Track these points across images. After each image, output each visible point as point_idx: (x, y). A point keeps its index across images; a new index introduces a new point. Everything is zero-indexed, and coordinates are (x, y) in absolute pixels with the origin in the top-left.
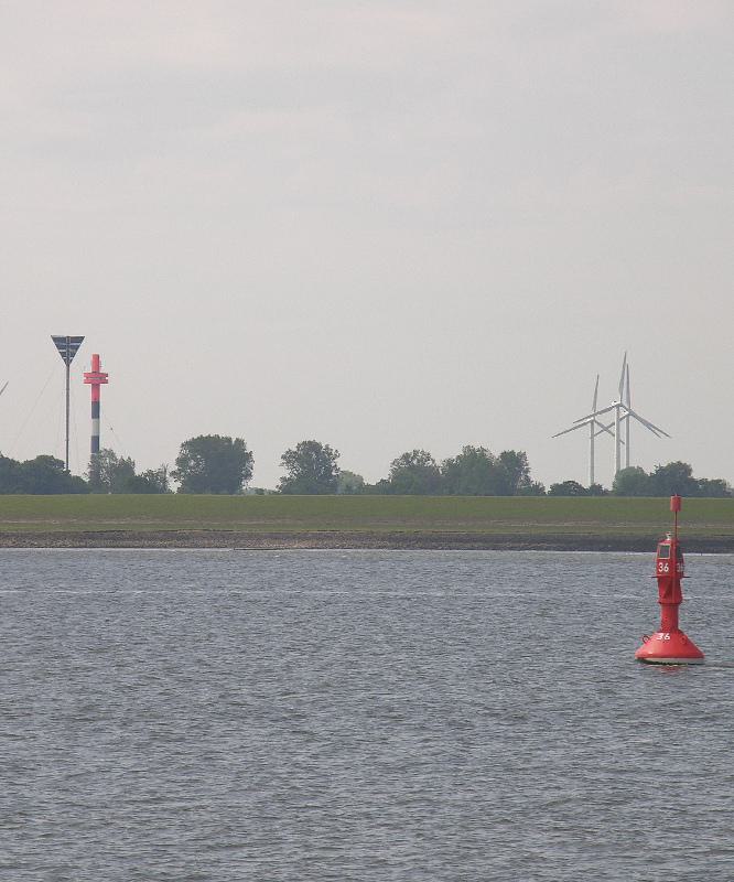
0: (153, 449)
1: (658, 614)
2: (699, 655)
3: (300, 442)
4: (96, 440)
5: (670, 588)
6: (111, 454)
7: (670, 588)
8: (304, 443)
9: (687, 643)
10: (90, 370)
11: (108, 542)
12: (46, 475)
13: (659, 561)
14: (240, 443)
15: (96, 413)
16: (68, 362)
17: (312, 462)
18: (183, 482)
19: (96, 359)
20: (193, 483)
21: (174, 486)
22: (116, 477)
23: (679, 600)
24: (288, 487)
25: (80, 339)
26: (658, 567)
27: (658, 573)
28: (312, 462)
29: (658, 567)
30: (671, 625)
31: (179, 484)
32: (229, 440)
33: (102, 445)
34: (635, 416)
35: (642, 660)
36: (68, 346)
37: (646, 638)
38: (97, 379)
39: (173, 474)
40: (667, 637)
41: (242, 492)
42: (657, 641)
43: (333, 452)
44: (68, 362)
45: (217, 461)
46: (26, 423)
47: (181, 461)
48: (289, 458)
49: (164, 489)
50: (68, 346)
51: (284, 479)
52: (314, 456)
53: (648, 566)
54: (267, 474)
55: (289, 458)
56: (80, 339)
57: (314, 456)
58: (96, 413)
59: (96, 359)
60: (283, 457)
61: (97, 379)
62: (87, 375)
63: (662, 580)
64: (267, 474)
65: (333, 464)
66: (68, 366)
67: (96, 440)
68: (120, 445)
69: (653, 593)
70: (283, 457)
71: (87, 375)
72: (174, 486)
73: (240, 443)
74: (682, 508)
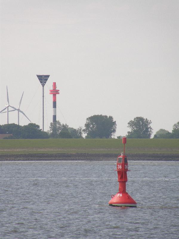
0: (76, 119)
1: (118, 186)
2: (135, 203)
3: (88, 117)
4: (55, 117)
5: (123, 175)
6: (59, 123)
7: (123, 175)
8: (137, 118)
9: (129, 197)
10: (52, 89)
11: (54, 158)
12: (32, 131)
13: (118, 164)
14: (111, 118)
15: (55, 106)
16: (43, 86)
17: (140, 126)
18: (88, 134)
19: (55, 84)
20: (92, 134)
21: (84, 135)
22: (64, 133)
23: (126, 180)
24: (130, 135)
25: (48, 76)
26: (118, 167)
27: (118, 169)
28: (140, 126)
29: (118, 167)
30: (123, 190)
31: (86, 135)
32: (106, 117)
33: (57, 120)
34: (10, 106)
35: (111, 205)
36: (43, 79)
37: (112, 196)
38: (55, 92)
39: (84, 130)
40: (121, 195)
41: (111, 138)
42: (118, 197)
43: (149, 121)
44: (43, 86)
45: (102, 125)
46: (35, 113)
47: (87, 125)
48: (131, 124)
49: (81, 137)
50: (43, 79)
51: (129, 132)
52: (141, 123)
53: (112, 167)
54: (122, 130)
55: (131, 124)
56: (48, 76)
57: (141, 123)
58: (55, 106)
59: (55, 84)
60: (129, 123)
61: (55, 92)
62: (51, 91)
63: (119, 172)
64: (122, 130)
65: (149, 126)
66: (43, 87)
67: (55, 117)
68: (62, 120)
69: (116, 178)
70: (129, 123)
71: (51, 91)
72: (84, 135)
73: (111, 118)
74: (127, 142)
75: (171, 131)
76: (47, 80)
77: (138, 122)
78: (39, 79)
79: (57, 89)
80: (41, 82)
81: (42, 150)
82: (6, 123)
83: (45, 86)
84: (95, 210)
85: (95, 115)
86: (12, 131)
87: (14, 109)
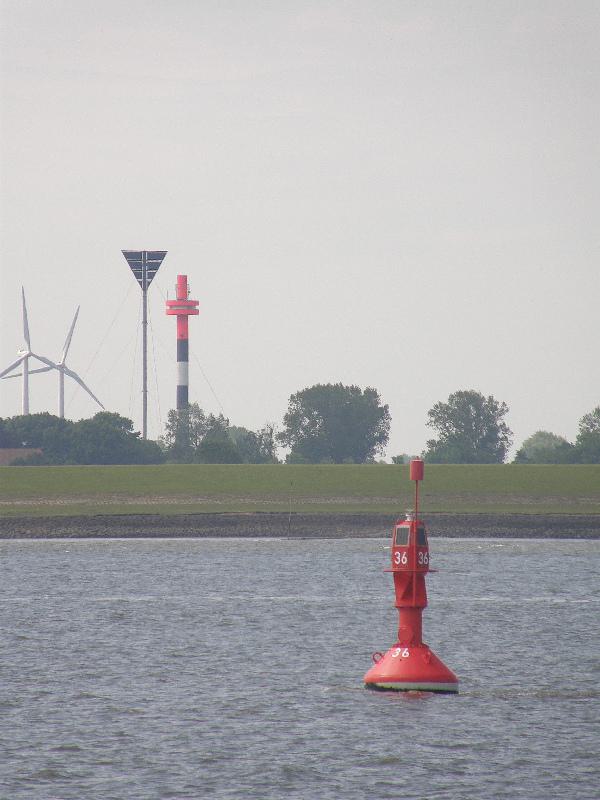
0: (254, 400)
1: (396, 623)
2: (451, 679)
3: (294, 393)
4: (183, 392)
5: (411, 586)
6: (198, 412)
7: (411, 586)
8: (460, 394)
9: (433, 661)
10: (174, 297)
11: (180, 530)
12: (108, 439)
13: (395, 549)
14: (372, 394)
15: (183, 354)
16: (145, 286)
17: (470, 421)
18: (293, 448)
19: (183, 281)
20: (308, 450)
21: (282, 452)
22: (213, 446)
23: (422, 603)
24: (437, 452)
25: (161, 255)
26: (394, 558)
27: (395, 565)
28: (470, 421)
29: (394, 558)
30: (412, 637)
31: (288, 451)
32: (356, 390)
33: (191, 401)
34: (34, 355)
35: (372, 686)
36: (144, 264)
37: (377, 657)
38: (184, 308)
39: (281, 436)
40: (406, 653)
41: (373, 461)
42: (394, 659)
43: (499, 407)
44: (145, 286)
45: (341, 419)
46: (116, 378)
47: (292, 420)
48: (440, 414)
49: (272, 458)
50: (144, 264)
51: (431, 443)
52: (473, 413)
53: (374, 559)
54: (409, 437)
55: (440, 414)
56: (161, 255)
57: (473, 413)
58: (183, 354)
59: (183, 281)
60: (431, 413)
61: (184, 308)
62: (171, 304)
63: (399, 577)
64: (409, 437)
65: (499, 423)
66: (145, 290)
67: (183, 392)
68: (209, 402)
69: (388, 595)
70: (431, 413)
71: (171, 304)
72: (282, 452)
73: (372, 394)
74: (425, 476)
75: (572, 438)
76: (156, 267)
77: (463, 407)
78: (132, 265)
79: (191, 297)
80: (138, 276)
81: (142, 502)
82: (22, 413)
83: (150, 289)
84: (320, 705)
85: (319, 386)
86: (39, 439)
87: (46, 366)
